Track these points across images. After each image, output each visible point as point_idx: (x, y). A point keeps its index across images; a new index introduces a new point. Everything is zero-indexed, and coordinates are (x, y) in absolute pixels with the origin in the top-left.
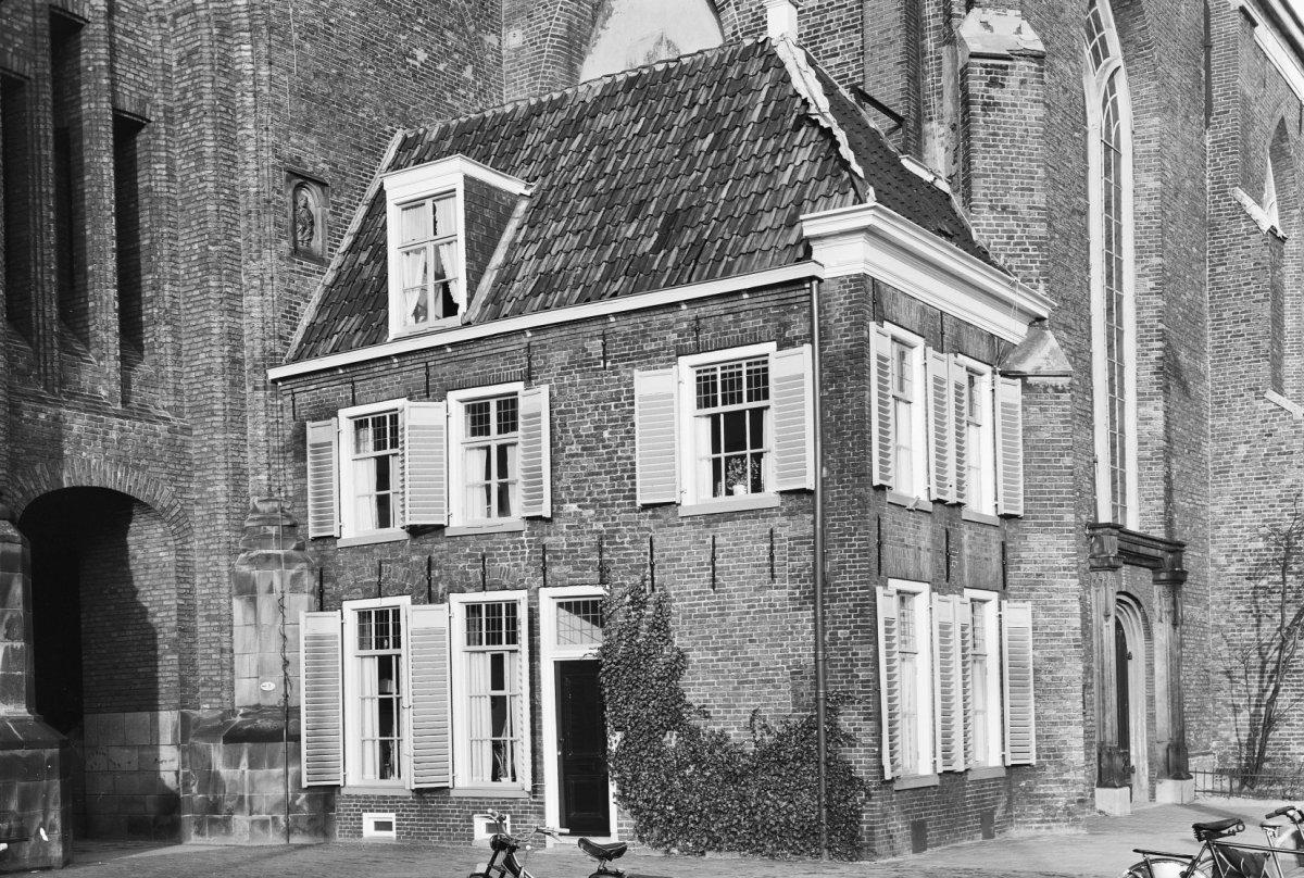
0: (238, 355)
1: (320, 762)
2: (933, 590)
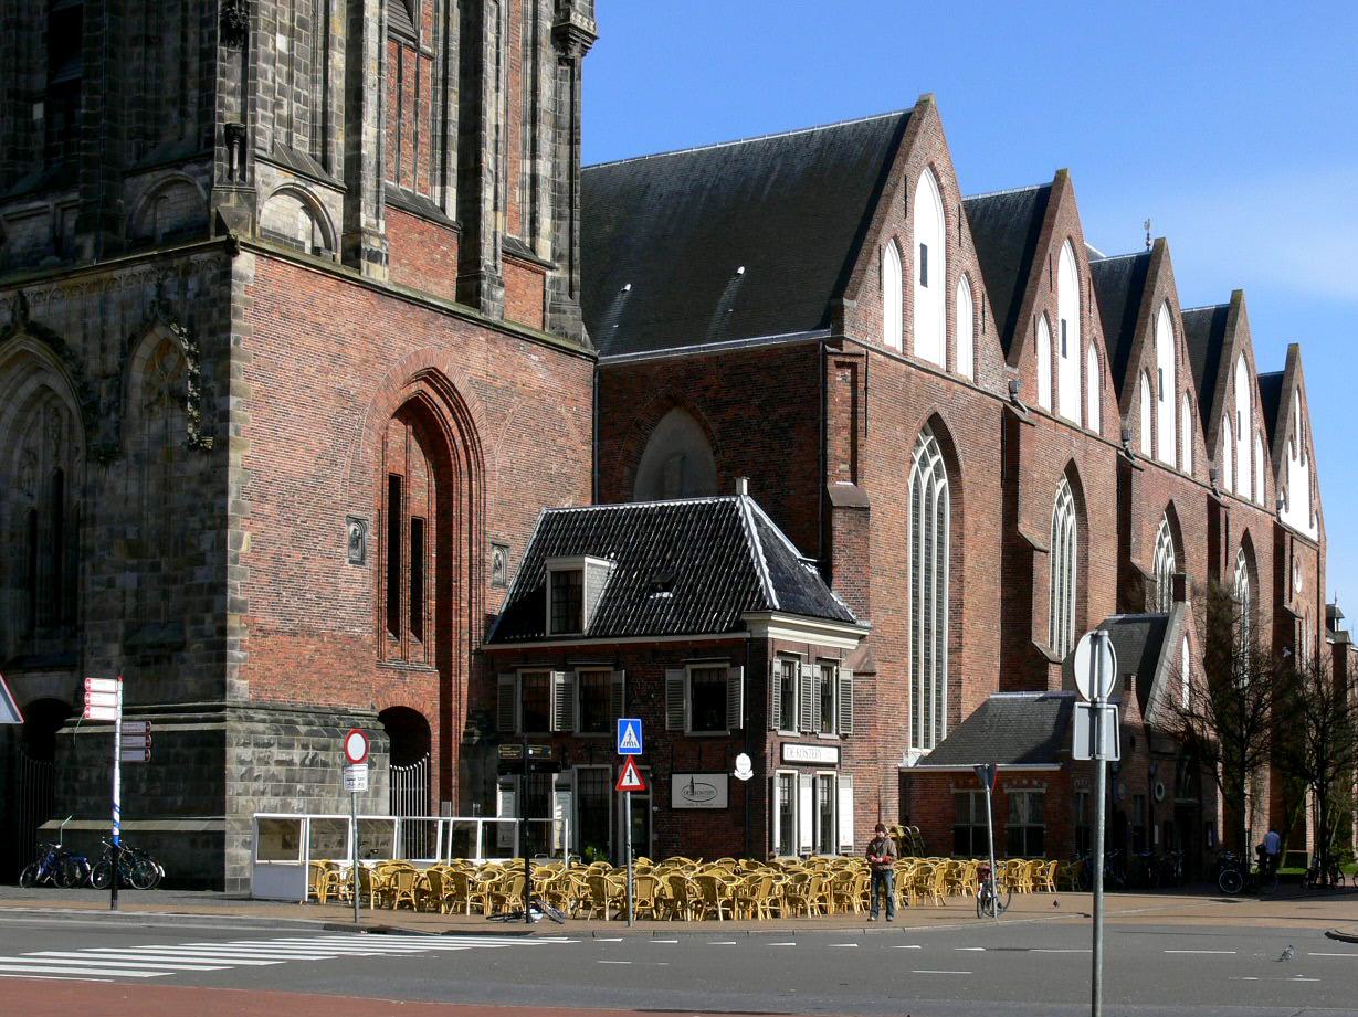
1: (692, 412)
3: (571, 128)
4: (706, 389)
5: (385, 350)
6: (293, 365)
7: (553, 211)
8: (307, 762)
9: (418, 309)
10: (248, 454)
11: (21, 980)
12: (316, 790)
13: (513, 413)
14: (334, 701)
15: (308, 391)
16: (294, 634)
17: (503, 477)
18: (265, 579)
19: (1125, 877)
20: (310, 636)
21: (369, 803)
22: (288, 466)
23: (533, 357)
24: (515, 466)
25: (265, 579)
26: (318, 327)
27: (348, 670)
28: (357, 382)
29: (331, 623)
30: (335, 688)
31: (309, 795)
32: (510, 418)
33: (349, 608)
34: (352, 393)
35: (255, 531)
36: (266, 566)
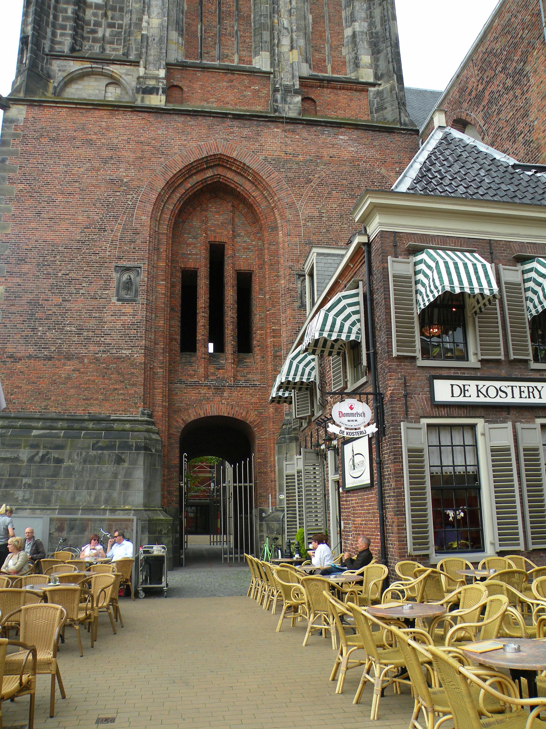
0: (278, 354)
2: (486, 422)
3: (540, 205)
4: (470, 94)
5: (163, 149)
6: (62, 168)
7: (372, 50)
8: (37, 458)
9: (200, 118)
10: (9, 231)
11: (478, 519)
12: (46, 484)
13: (319, 177)
14: (95, 410)
15: (77, 184)
16: (50, 358)
17: (309, 224)
18: (19, 319)
19: (322, 432)
20: (69, 359)
21: (115, 495)
22: (50, 236)
23: (341, 137)
24: (324, 215)
25: (19, 319)
26: (90, 143)
27: (113, 384)
28: (132, 173)
29: (92, 348)
30: (97, 399)
31: (38, 487)
32: (316, 181)
33: (115, 335)
34: (125, 180)
35: (10, 285)
36: (21, 309)
